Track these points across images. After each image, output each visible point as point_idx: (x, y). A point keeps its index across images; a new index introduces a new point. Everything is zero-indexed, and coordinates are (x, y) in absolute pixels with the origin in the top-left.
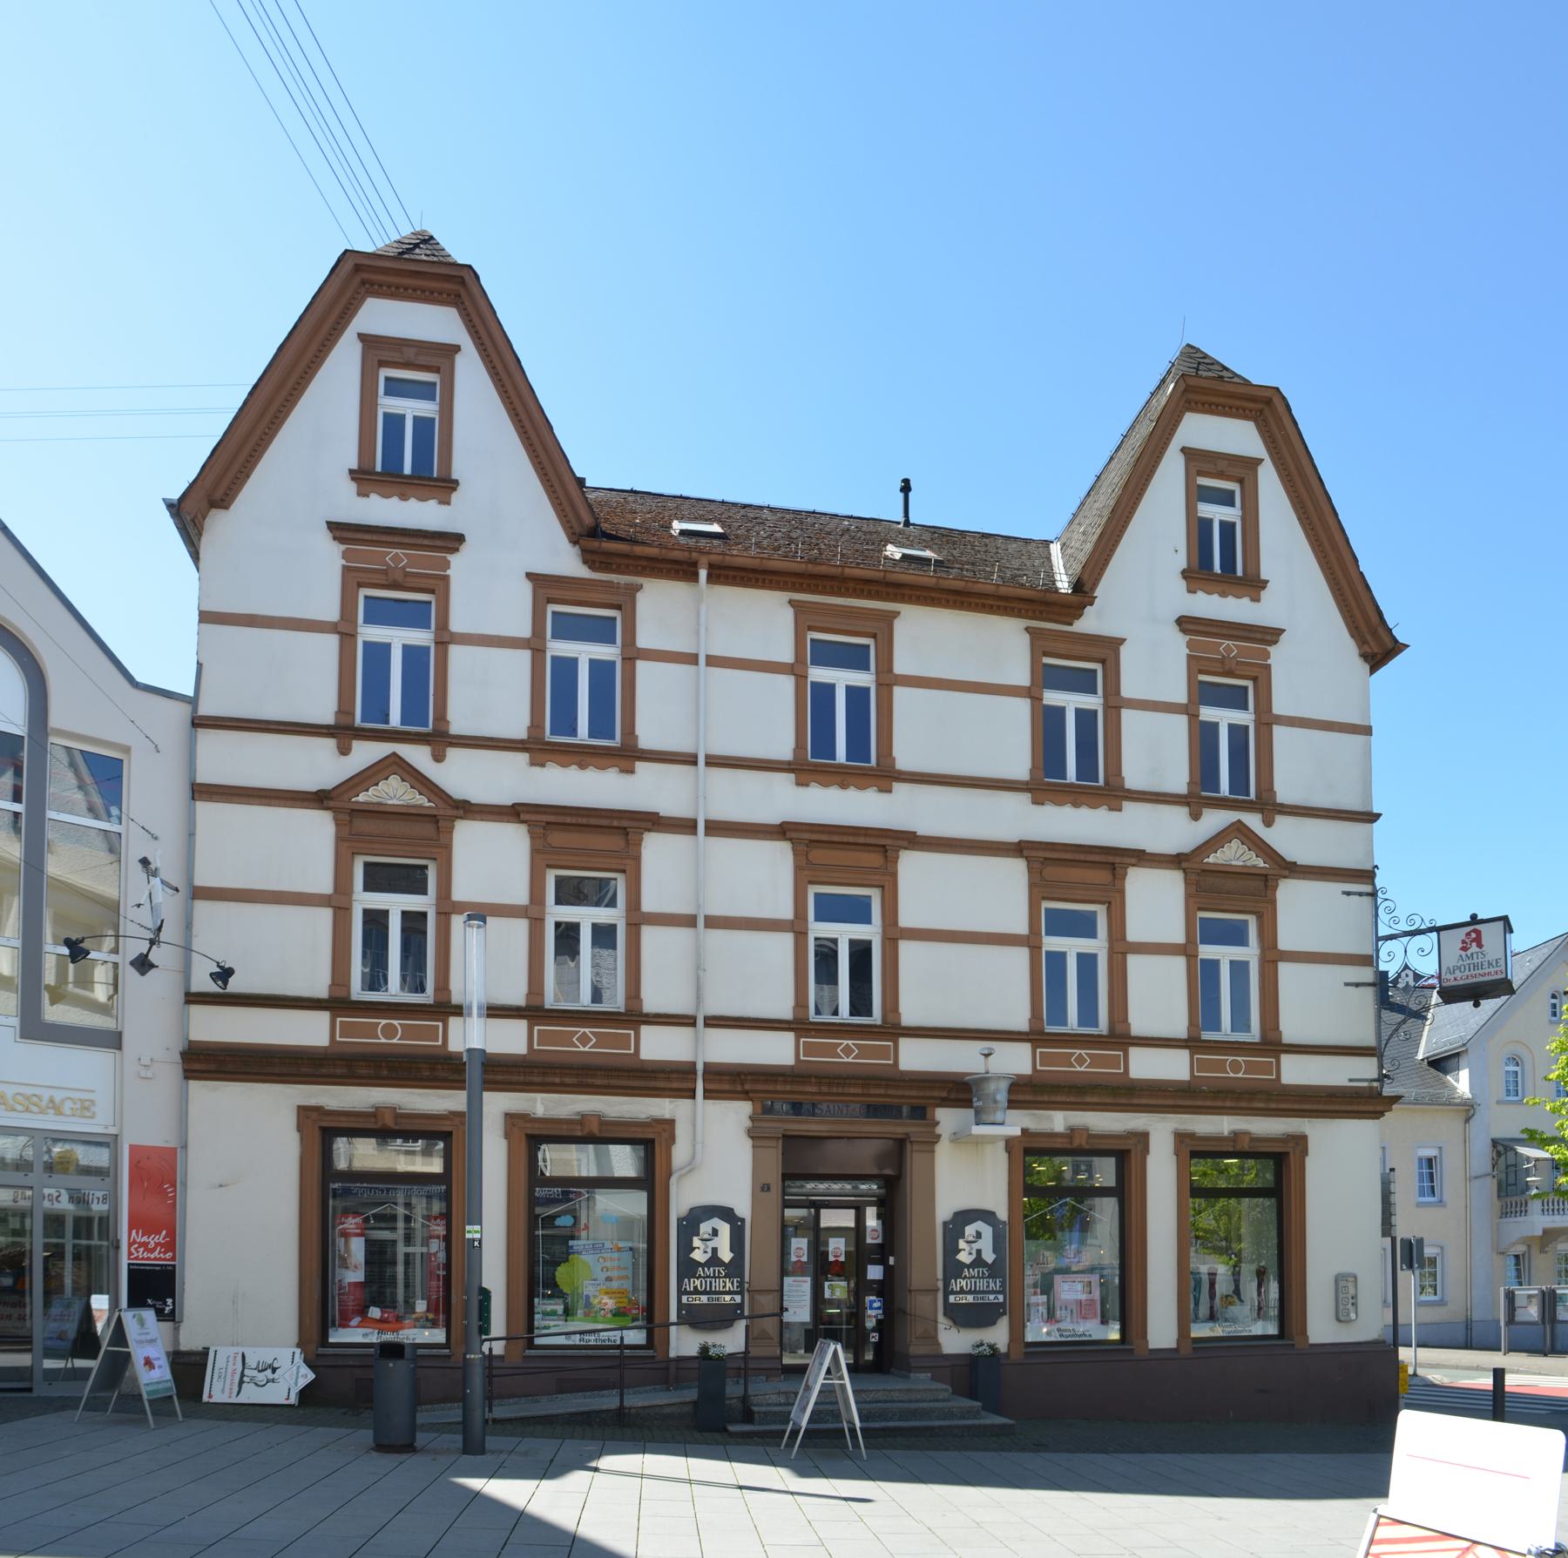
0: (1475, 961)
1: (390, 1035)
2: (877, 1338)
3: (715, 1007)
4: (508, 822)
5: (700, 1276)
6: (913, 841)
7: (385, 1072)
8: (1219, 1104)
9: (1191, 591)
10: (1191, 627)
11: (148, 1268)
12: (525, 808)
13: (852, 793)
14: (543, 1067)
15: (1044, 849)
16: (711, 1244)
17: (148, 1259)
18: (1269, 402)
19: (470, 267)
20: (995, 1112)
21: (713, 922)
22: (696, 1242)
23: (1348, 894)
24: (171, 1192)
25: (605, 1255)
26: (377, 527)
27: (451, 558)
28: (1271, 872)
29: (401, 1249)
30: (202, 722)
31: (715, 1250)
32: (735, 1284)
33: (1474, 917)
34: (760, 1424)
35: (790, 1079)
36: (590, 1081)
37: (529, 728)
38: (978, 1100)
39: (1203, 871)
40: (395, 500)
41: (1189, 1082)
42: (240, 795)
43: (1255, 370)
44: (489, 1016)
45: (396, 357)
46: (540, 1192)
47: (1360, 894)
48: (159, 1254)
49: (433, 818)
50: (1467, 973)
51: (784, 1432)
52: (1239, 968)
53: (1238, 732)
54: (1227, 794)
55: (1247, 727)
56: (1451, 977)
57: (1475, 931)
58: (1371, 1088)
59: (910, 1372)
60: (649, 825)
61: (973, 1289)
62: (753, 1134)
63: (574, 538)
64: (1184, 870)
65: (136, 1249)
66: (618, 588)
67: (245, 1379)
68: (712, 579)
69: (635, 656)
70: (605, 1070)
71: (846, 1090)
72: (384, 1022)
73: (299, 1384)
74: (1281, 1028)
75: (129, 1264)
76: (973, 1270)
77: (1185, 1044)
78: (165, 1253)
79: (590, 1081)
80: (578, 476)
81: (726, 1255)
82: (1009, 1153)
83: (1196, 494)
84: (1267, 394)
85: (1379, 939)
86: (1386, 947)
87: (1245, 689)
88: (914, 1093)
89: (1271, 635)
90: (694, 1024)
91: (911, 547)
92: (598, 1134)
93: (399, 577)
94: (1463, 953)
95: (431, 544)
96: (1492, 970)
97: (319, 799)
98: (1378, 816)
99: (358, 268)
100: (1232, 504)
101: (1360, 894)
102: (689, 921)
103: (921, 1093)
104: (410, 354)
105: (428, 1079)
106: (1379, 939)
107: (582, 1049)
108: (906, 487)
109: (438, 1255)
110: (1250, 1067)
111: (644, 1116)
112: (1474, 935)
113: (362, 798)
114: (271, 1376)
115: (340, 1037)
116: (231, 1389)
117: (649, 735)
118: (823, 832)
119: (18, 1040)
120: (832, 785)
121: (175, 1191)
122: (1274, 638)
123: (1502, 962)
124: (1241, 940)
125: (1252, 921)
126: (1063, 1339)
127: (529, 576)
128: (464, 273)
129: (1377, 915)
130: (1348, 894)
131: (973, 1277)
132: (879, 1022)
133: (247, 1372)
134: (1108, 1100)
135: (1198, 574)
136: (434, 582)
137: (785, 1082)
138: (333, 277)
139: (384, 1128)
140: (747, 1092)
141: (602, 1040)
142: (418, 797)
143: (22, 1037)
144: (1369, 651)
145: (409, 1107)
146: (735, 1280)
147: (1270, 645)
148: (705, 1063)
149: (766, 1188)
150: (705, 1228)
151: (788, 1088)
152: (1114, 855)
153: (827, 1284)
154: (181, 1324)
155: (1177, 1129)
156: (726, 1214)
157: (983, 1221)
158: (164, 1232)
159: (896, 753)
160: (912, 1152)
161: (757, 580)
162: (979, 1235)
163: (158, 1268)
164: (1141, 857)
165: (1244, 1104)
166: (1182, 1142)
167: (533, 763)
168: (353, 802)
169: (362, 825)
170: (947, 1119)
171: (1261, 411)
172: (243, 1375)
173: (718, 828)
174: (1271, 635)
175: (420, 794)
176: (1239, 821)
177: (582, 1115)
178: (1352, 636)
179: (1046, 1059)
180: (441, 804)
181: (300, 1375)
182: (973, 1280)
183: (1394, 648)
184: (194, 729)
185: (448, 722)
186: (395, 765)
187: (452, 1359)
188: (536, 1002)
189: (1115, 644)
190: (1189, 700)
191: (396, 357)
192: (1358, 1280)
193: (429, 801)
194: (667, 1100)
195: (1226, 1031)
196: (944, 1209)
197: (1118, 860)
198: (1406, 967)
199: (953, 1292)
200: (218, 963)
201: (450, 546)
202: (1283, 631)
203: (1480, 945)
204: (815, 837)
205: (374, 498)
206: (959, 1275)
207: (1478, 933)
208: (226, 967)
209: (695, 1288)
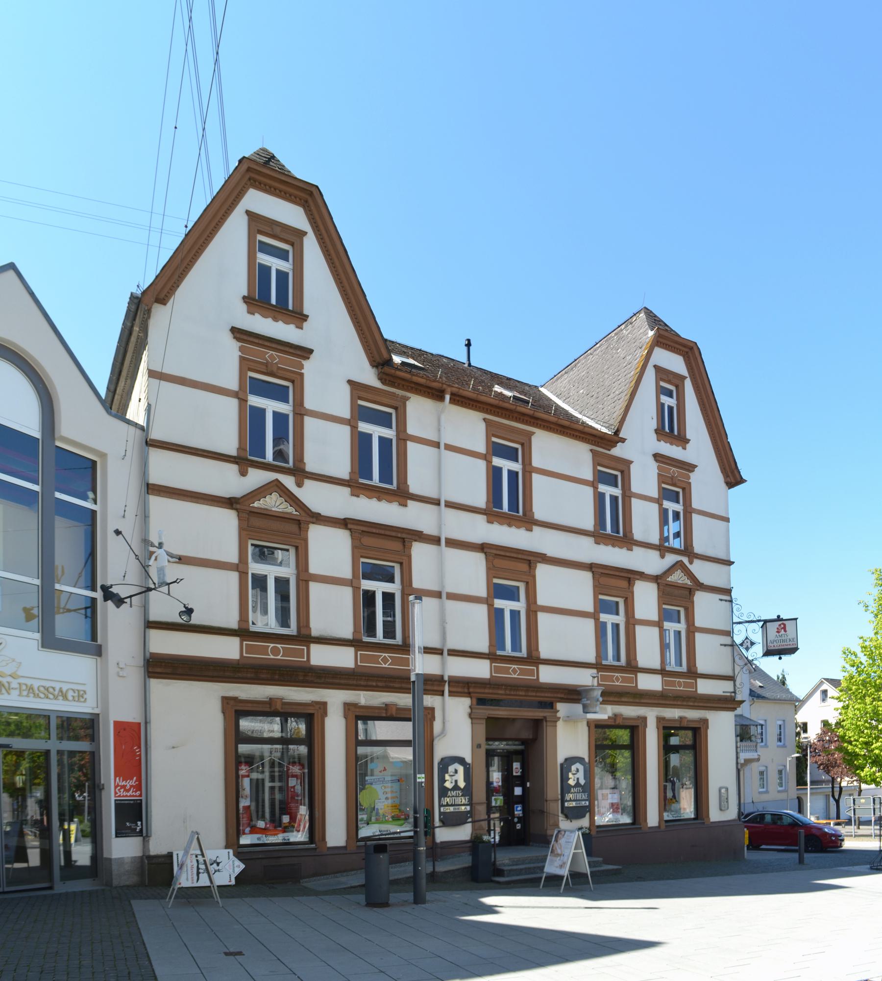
0: (783, 638)
1: (276, 653)
3: (452, 644)
4: (339, 528)
5: (449, 797)
6: (419, 536)
7: (277, 677)
8: (675, 703)
9: (659, 440)
10: (660, 459)
11: (126, 802)
12: (352, 522)
13: (513, 530)
14: (368, 676)
15: (602, 568)
16: (454, 778)
17: (126, 796)
18: (691, 349)
19: (317, 187)
20: (596, 706)
21: (452, 597)
22: (447, 777)
23: (721, 600)
24: (138, 752)
25: (385, 785)
26: (263, 336)
28: (694, 587)
29: (268, 784)
30: (154, 444)
31: (456, 781)
33: (779, 616)
34: (508, 876)
35: (492, 686)
36: (391, 685)
38: (588, 700)
39: (666, 584)
41: (490, 679)
42: (184, 495)
43: (685, 332)
44: (425, 652)
45: (267, 229)
47: (726, 601)
48: (133, 792)
49: (298, 522)
50: (779, 644)
51: (541, 878)
52: (515, 614)
53: (385, 443)
54: (610, 532)
55: (391, 440)
56: (772, 645)
57: (783, 624)
58: (731, 696)
60: (417, 538)
64: (593, 572)
65: (119, 790)
66: (397, 397)
67: (201, 871)
70: (365, 676)
71: (518, 693)
72: (272, 645)
73: (236, 872)
74: (697, 665)
75: (115, 800)
77: (487, 657)
78: (136, 792)
79: (391, 685)
81: (462, 784)
82: (346, 718)
83: (254, 248)
84: (692, 345)
85: (733, 623)
86: (737, 628)
87: (517, 449)
88: (549, 695)
89: (306, 353)
90: (442, 654)
91: (408, 357)
92: (395, 716)
93: (275, 369)
94: (778, 634)
95: (294, 352)
96: (791, 643)
97: (230, 503)
98: (733, 563)
99: (249, 169)
100: (287, 260)
101: (726, 601)
102: (438, 595)
103: (552, 695)
104: (277, 230)
105: (303, 682)
106: (733, 623)
107: (384, 666)
109: (296, 787)
110: (523, 672)
112: (782, 626)
113: (256, 504)
114: (217, 868)
116: (192, 878)
117: (415, 485)
118: (500, 550)
119: (40, 649)
121: (140, 751)
123: (795, 640)
124: (391, 580)
125: (397, 568)
126: (674, 818)
128: (313, 190)
129: (732, 611)
130: (721, 600)
131: (453, 796)
134: (631, 700)
135: (661, 433)
136: (294, 375)
137: (490, 688)
138: (236, 171)
139: (266, 709)
142: (289, 508)
143: (43, 647)
144: (729, 480)
145: (290, 698)
149: (479, 746)
150: (451, 769)
151: (491, 691)
152: (631, 574)
153: (493, 798)
154: (151, 838)
156: (461, 761)
158: (135, 778)
159: (410, 482)
161: (469, 404)
162: (578, 770)
163: (132, 802)
164: (642, 576)
165: (685, 703)
166: (660, 722)
167: (353, 495)
168: (251, 507)
169: (256, 522)
170: (562, 708)
171: (687, 352)
173: (453, 543)
174: (306, 353)
175: (291, 506)
176: (277, 480)
177: (270, 699)
178: (722, 472)
179: (250, 649)
180: (303, 514)
181: (235, 865)
182: (453, 798)
184: (147, 448)
185: (305, 463)
186: (277, 487)
187: (318, 850)
188: (244, 626)
189: (628, 463)
190: (352, 416)
191: (267, 229)
192: (729, 790)
193: (296, 511)
194: (429, 696)
196: (560, 759)
197: (632, 576)
198: (747, 638)
199: (567, 801)
200: (185, 605)
201: (305, 355)
202: (697, 466)
203: (785, 631)
206: (569, 792)
207: (785, 625)
208: (189, 607)
209: (447, 802)
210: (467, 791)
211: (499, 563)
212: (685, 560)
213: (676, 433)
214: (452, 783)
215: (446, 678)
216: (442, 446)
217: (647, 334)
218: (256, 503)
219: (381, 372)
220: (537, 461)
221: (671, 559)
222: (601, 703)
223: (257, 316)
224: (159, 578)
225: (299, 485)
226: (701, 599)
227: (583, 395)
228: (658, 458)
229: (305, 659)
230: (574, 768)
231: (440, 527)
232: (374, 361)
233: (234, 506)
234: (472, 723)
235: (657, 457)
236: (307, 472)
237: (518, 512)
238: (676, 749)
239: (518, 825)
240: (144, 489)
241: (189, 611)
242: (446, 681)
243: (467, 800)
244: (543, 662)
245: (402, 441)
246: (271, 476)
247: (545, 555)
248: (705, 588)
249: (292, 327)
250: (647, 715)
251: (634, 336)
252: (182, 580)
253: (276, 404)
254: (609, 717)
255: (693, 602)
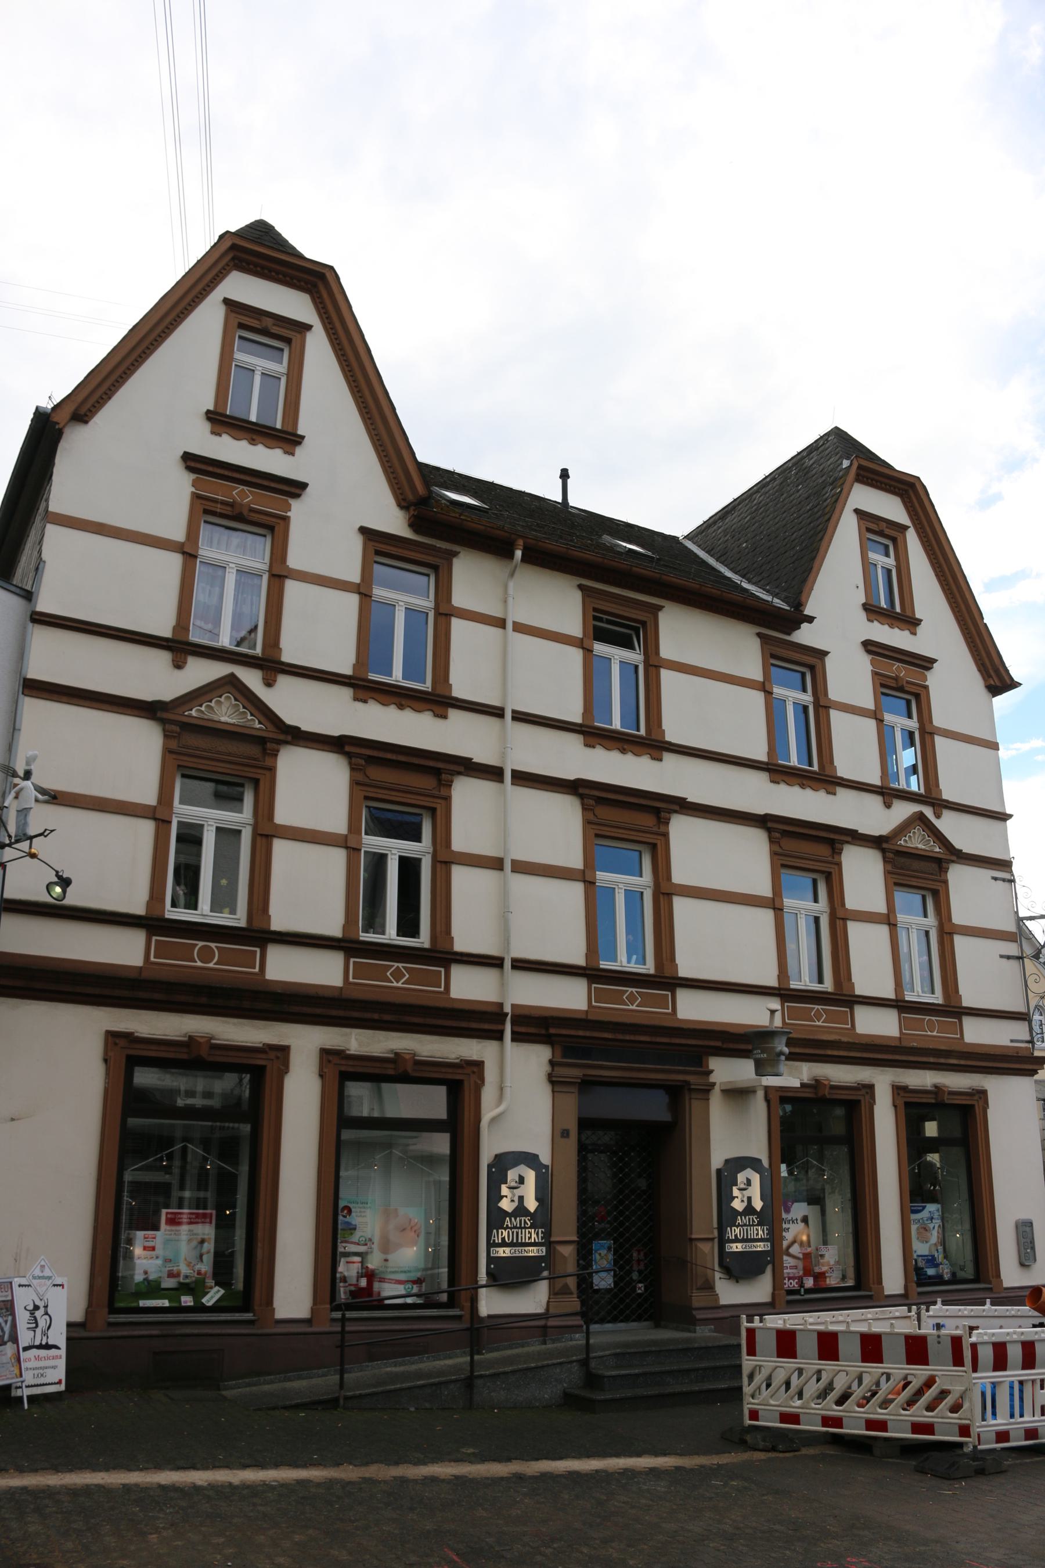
2: (643, 1289)
5: (739, 1225)
16: (747, 1193)
19: (332, 268)
21: (522, 868)
22: (504, 1190)
23: (995, 879)
27: (292, 502)
31: (521, 1199)
32: (766, 1232)
37: (354, 665)
40: (244, 443)
46: (347, 1135)
49: (260, 741)
59: (695, 1325)
61: (745, 1237)
62: (553, 1081)
63: (403, 504)
68: (525, 559)
69: (286, 574)
72: (201, 944)
76: (515, 1219)
80: (421, 458)
81: (532, 1205)
84: (912, 480)
89: (295, 488)
98: (1010, 816)
102: (496, 864)
107: (395, 984)
108: (565, 475)
111: (453, 1056)
115: (155, 958)
120: (614, 749)
122: (297, 491)
127: (363, 530)
130: (995, 879)
132: (427, 945)
133: (37, 1343)
136: (274, 520)
140: (550, 1036)
141: (646, 1001)
144: (992, 683)
145: (226, 1037)
146: (540, 1230)
147: (926, 670)
148: (512, 1005)
149: (565, 1134)
150: (512, 1175)
155: (893, 1082)
156: (530, 1159)
157: (524, 1164)
159: (666, 725)
160: (690, 1099)
168: (186, 716)
172: (40, 1347)
173: (523, 778)
176: (232, 675)
178: (979, 670)
180: (271, 728)
182: (745, 1228)
183: (1011, 685)
185: (281, 649)
188: (156, 913)
189: (823, 654)
193: (260, 723)
195: (623, 961)
196: (717, 1161)
200: (57, 872)
204: (375, 753)
205: (226, 438)
206: (501, 1226)
208: (65, 876)
209: (736, 1236)
210: (542, 1219)
211: (790, 845)
212: (928, 812)
213: (898, 609)
214: (513, 1201)
215: (508, 1009)
216: (509, 625)
217: (841, 464)
218: (194, 710)
219: (413, 515)
220: (667, 650)
221: (903, 811)
222: (787, 1059)
223: (876, 623)
224: (18, 827)
225: (269, 683)
226: (958, 877)
227: (747, 550)
228: (870, 648)
229: (257, 970)
230: (741, 1177)
231: (503, 755)
232: (404, 500)
233: (159, 714)
234: (553, 1092)
235: (870, 646)
236: (283, 663)
237: (638, 730)
238: (933, 1145)
239: (640, 1285)
240: (18, 686)
241: (65, 883)
242: (506, 1014)
243: (540, 1235)
244: (458, 958)
245: (654, 668)
246: (217, 670)
247: (856, 831)
248: (966, 859)
249: (278, 452)
250: (874, 1081)
251: (822, 467)
252: (52, 831)
253: (624, 653)
254: (803, 1085)
255: (946, 882)
